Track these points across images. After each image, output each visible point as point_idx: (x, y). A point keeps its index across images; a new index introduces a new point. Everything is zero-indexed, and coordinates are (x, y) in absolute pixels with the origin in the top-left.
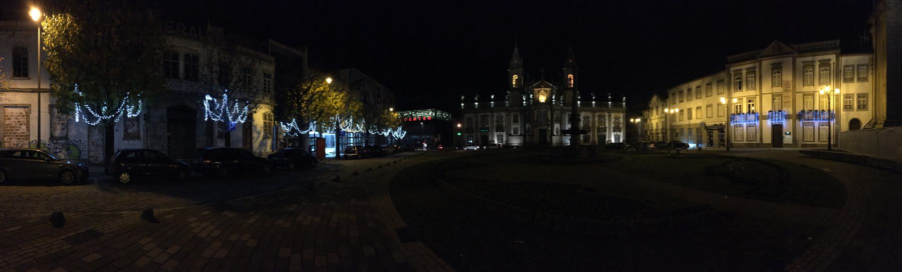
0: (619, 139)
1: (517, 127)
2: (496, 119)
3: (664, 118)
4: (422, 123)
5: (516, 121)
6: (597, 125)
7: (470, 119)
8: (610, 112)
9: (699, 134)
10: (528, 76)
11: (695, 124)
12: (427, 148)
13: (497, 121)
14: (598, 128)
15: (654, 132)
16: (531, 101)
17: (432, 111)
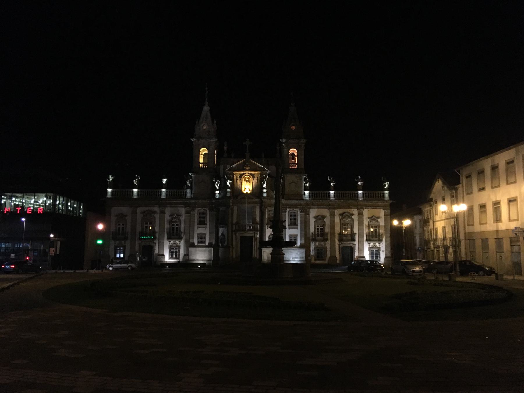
1: (204, 232)
2: (169, 218)
4: (23, 219)
5: (202, 223)
6: (338, 229)
7: (121, 217)
8: (360, 207)
9: (516, 248)
10: (225, 148)
11: (507, 230)
12: (120, 258)
13: (170, 222)
14: (341, 234)
15: (439, 243)
16: (228, 190)
17: (46, 197)
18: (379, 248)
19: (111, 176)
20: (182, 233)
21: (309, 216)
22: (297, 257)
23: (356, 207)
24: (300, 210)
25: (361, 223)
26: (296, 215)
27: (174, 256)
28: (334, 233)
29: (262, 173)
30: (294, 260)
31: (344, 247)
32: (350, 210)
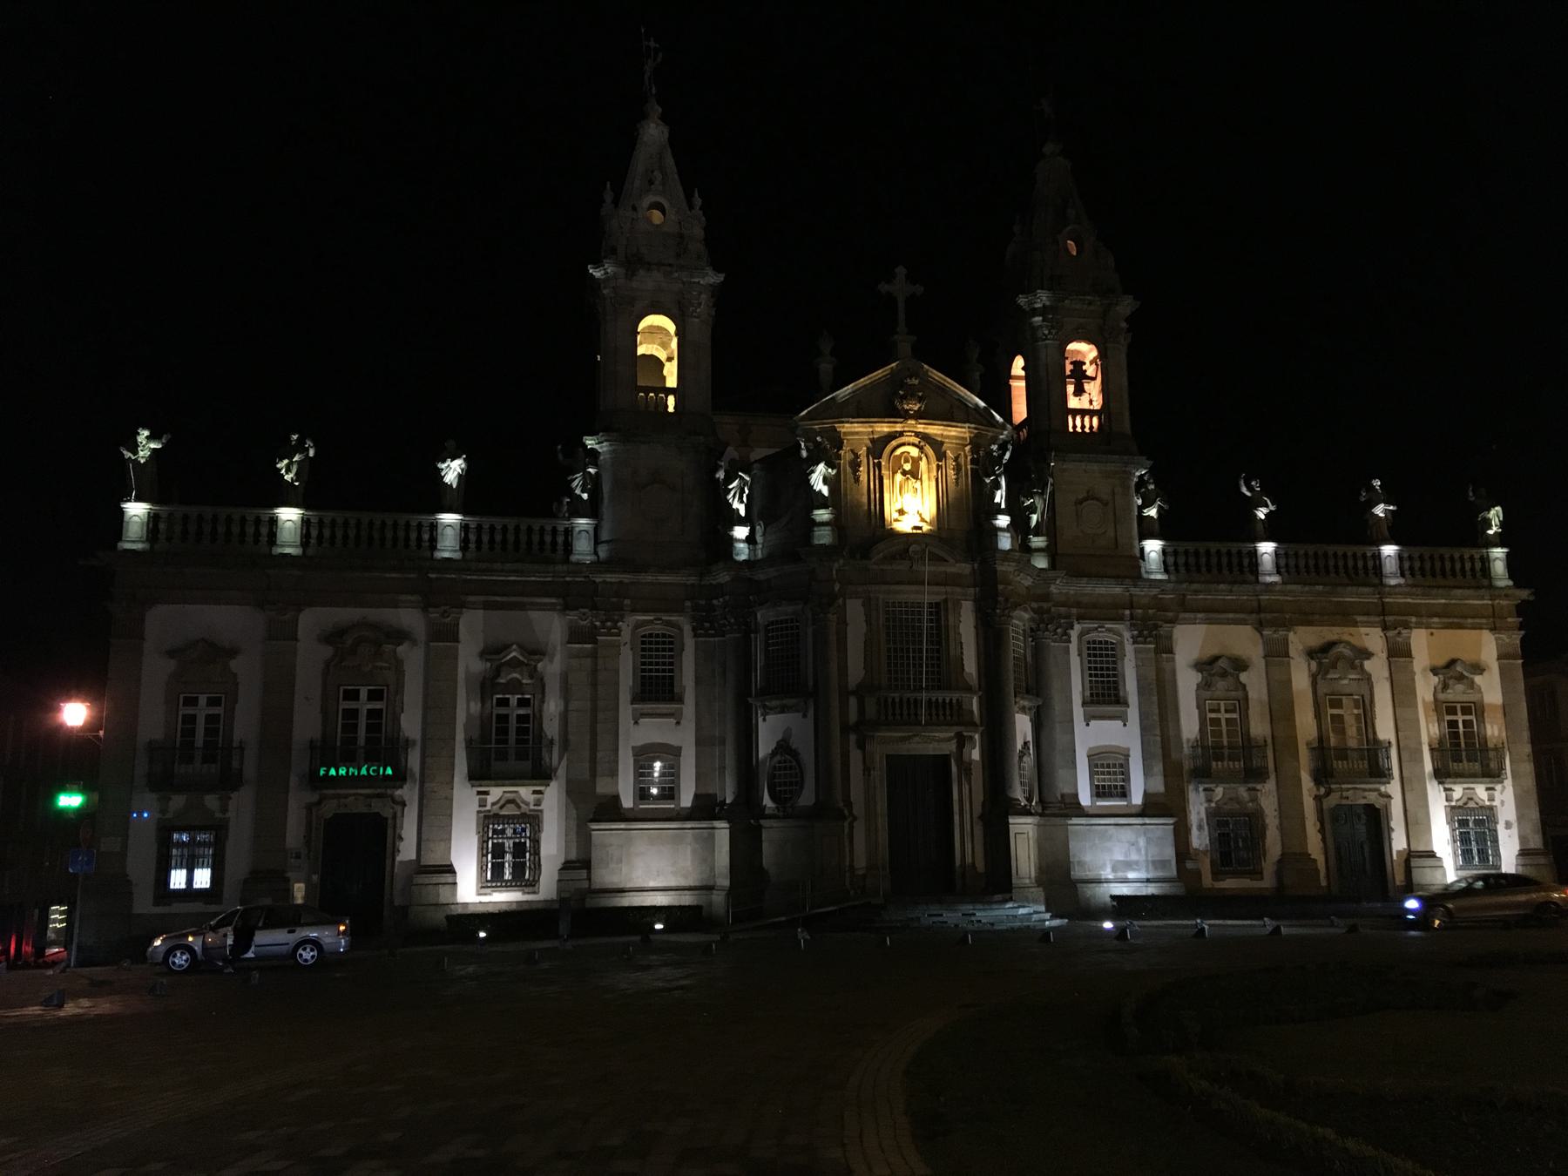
2: (480, 667)
6: (1306, 725)
8: (1394, 619)
12: (190, 893)
13: (486, 687)
14: (1320, 748)
16: (822, 515)
18: (1491, 808)
19: (146, 433)
20: (551, 742)
21: (1173, 660)
22: (1137, 863)
23: (1377, 619)
24: (1133, 626)
25: (1402, 694)
26: (1113, 656)
27: (507, 876)
28: (1293, 740)
29: (976, 436)
30: (1120, 874)
31: (1339, 806)
32: (1352, 630)
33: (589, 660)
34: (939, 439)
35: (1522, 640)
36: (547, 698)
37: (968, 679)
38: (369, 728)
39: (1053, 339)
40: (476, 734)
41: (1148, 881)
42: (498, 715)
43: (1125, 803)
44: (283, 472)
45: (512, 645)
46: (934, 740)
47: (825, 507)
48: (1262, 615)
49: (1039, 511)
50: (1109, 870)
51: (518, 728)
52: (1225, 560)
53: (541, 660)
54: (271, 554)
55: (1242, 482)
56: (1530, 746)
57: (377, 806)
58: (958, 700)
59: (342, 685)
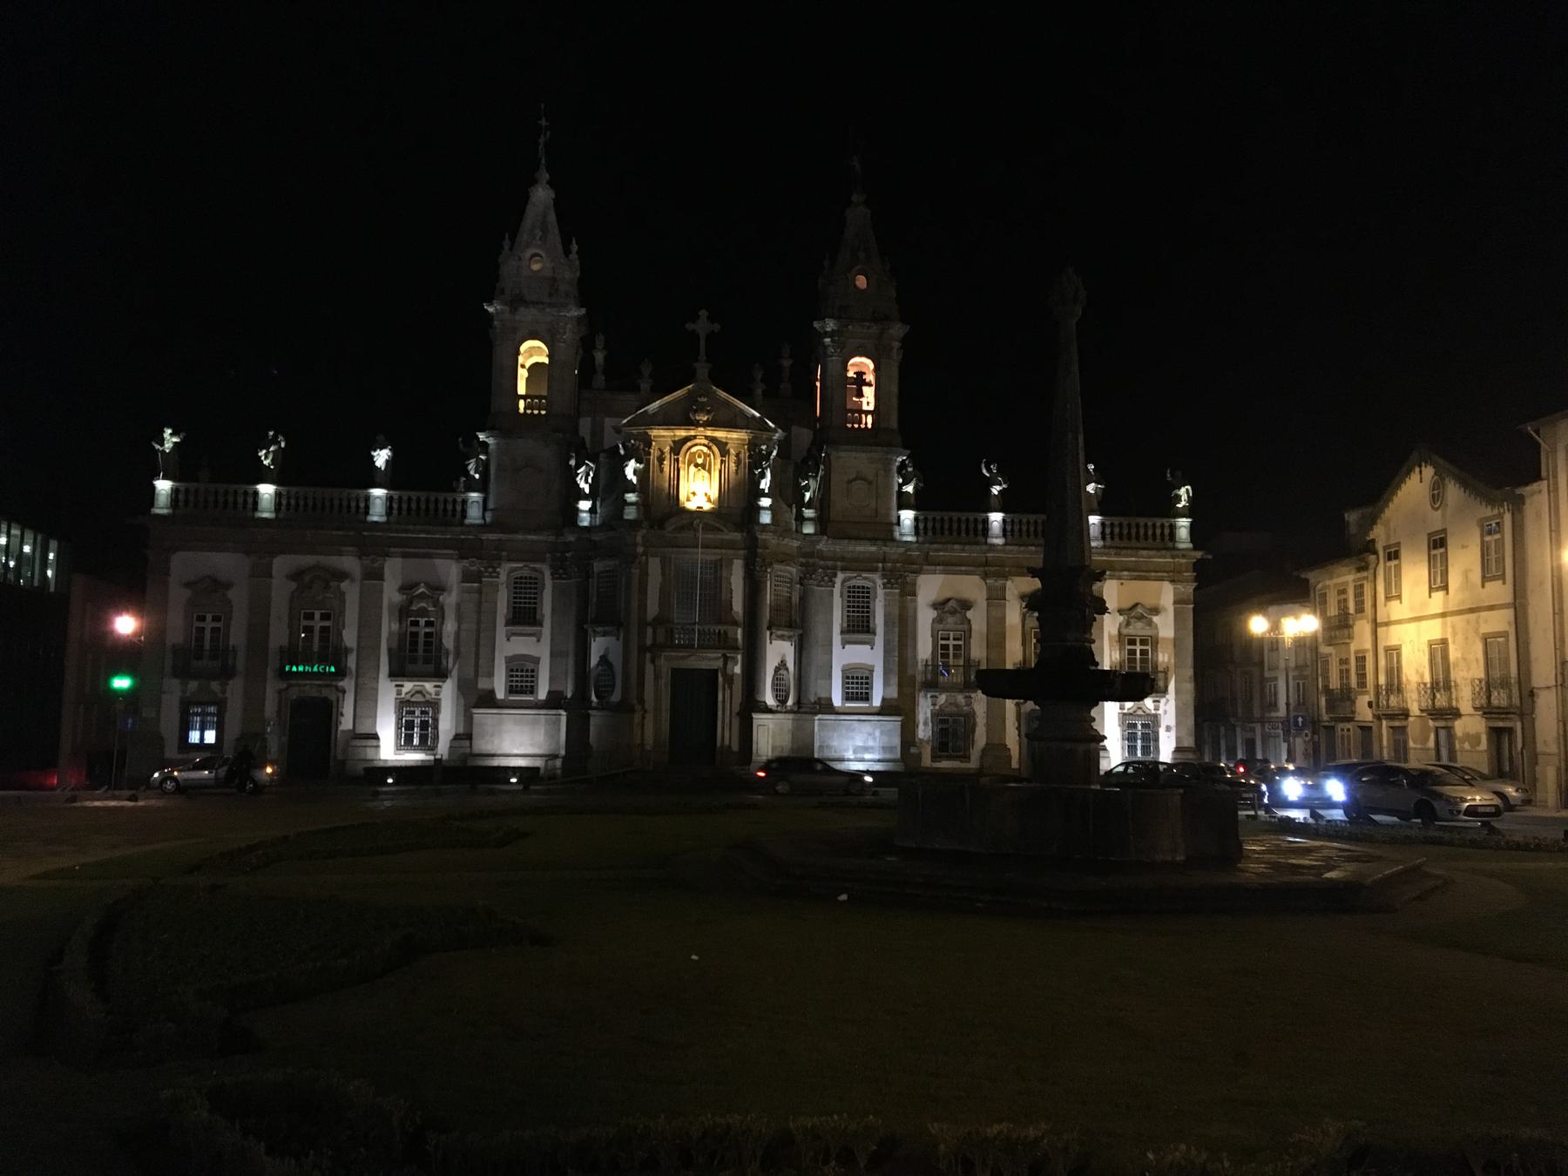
0: (1151, 739)
2: (398, 598)
3: (1509, 614)
5: (524, 617)
7: (210, 588)
12: (201, 746)
13: (403, 612)
16: (631, 497)
18: (1156, 716)
19: (169, 431)
21: (915, 601)
22: (872, 748)
24: (884, 576)
26: (868, 597)
27: (416, 741)
30: (859, 756)
33: (476, 595)
34: (724, 441)
35: (1195, 590)
36: (445, 622)
37: (735, 616)
38: (321, 639)
39: (838, 356)
40: (395, 645)
41: (879, 761)
42: (411, 632)
43: (867, 705)
44: (263, 458)
45: (420, 583)
46: (704, 659)
47: (633, 492)
48: (986, 568)
49: (811, 490)
50: (851, 752)
51: (425, 642)
52: (963, 527)
53: (442, 594)
54: (253, 517)
55: (983, 465)
56: (1192, 670)
57: (325, 692)
58: (725, 632)
59: (303, 609)
